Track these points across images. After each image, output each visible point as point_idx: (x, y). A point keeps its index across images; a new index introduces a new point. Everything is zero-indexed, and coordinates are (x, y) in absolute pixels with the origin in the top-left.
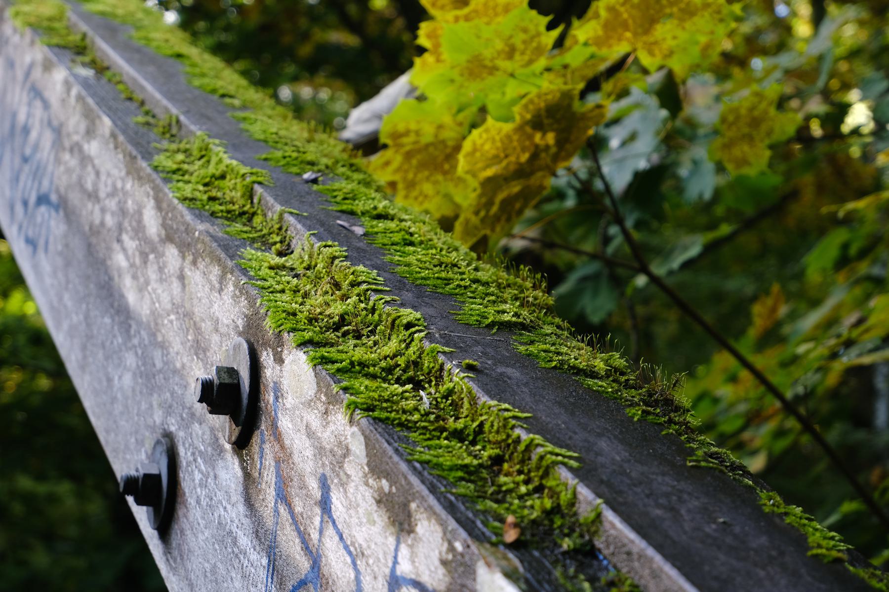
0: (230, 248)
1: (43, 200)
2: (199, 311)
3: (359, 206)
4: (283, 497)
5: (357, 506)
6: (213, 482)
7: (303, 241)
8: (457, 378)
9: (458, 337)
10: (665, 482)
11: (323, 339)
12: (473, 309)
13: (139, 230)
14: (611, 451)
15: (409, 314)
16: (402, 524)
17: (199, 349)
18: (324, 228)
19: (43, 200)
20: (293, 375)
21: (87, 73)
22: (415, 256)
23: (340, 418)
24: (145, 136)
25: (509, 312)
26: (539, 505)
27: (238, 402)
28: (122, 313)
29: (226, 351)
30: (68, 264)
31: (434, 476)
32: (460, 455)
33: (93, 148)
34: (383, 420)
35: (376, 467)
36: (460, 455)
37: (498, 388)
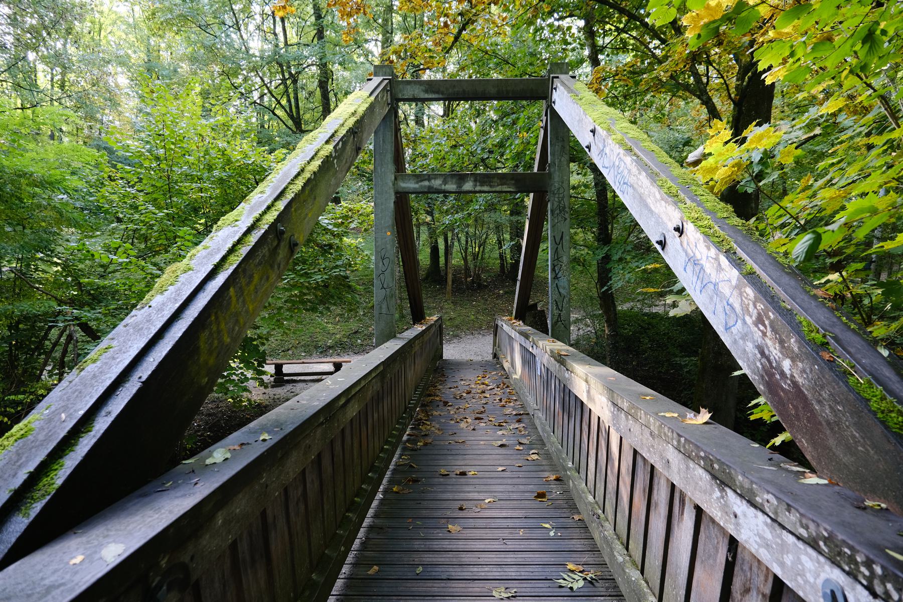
0: (676, 203)
1: (624, 183)
2: (671, 215)
3: (698, 193)
4: (688, 244)
5: (702, 246)
6: (673, 240)
7: (688, 202)
8: (716, 228)
9: (716, 220)
10: (747, 243)
11: (695, 221)
12: (719, 215)
13: (655, 196)
14: (740, 239)
15: (709, 217)
16: (709, 249)
17: (670, 220)
18: (693, 200)
19: (624, 183)
20: (689, 228)
21: (635, 158)
22: (709, 204)
23: (698, 234)
24: (653, 176)
25: (725, 215)
26: (728, 247)
27: (680, 230)
28: (651, 211)
29: (677, 222)
30: (634, 198)
31: (713, 243)
32: (717, 240)
33: (641, 177)
34: (706, 235)
35: (705, 241)
36: (717, 240)
37: (723, 230)
